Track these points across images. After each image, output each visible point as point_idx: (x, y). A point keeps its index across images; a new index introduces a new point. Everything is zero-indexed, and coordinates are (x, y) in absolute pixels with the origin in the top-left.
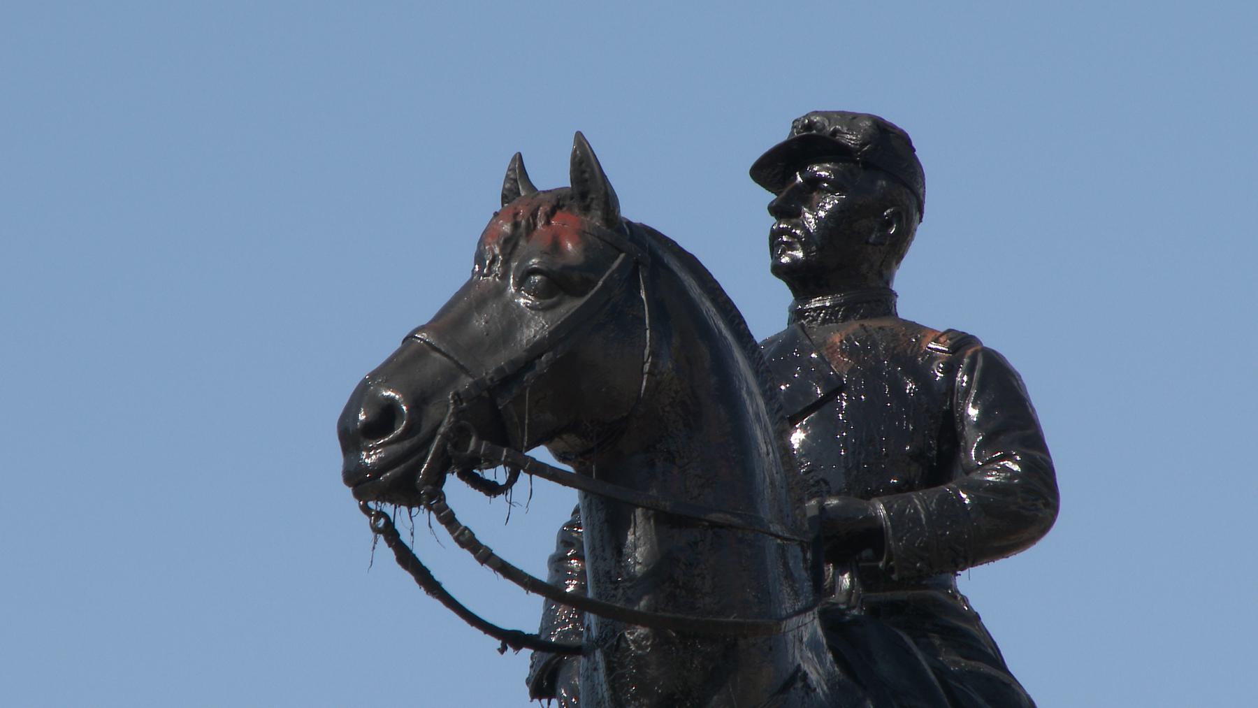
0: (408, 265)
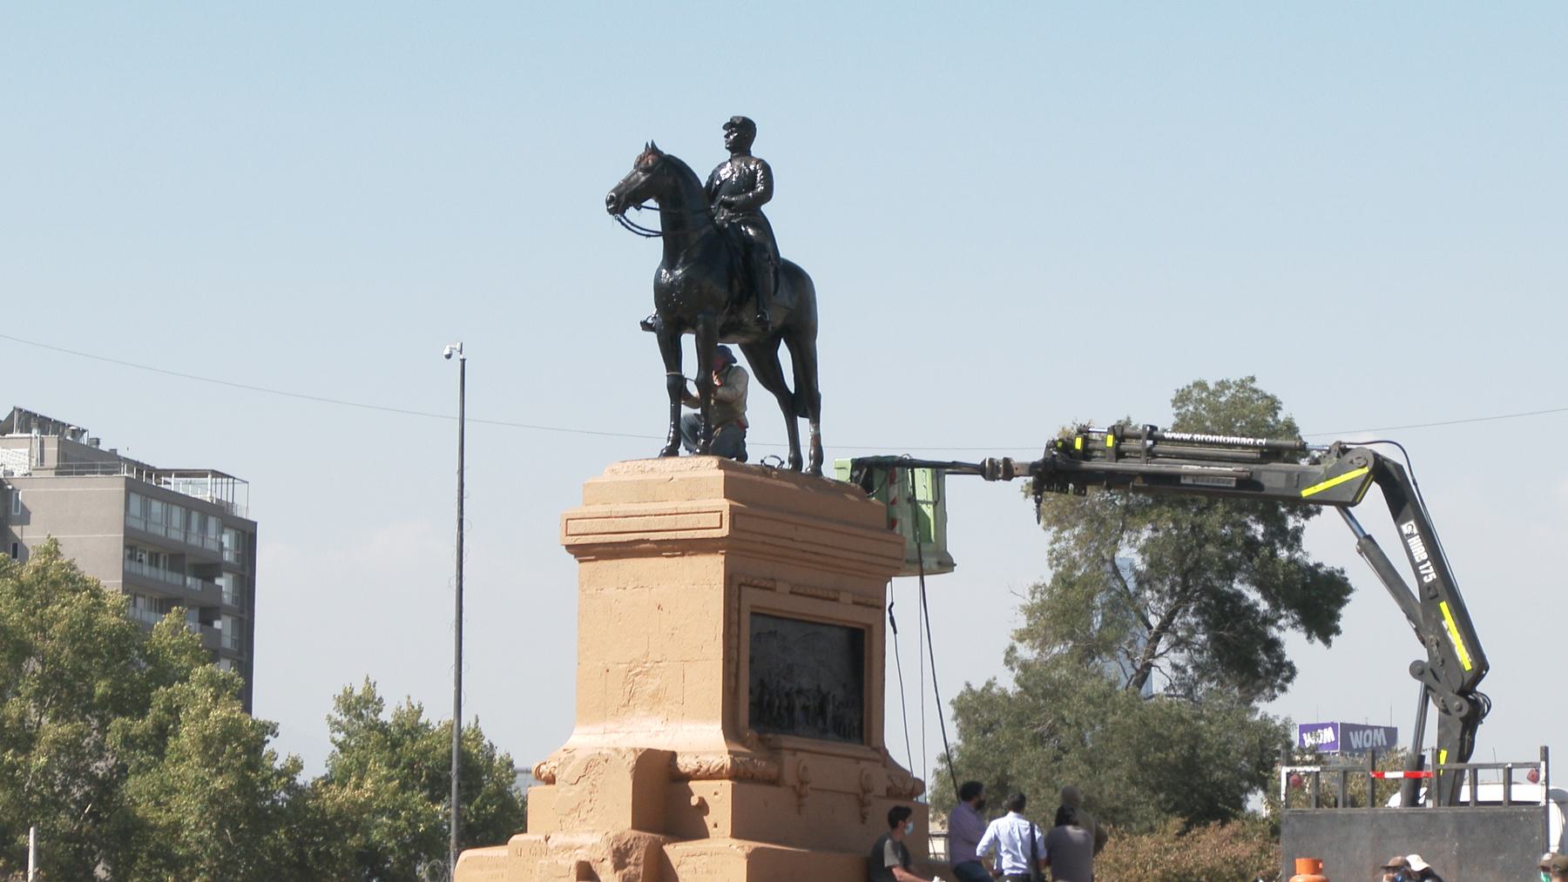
0: (622, 167)
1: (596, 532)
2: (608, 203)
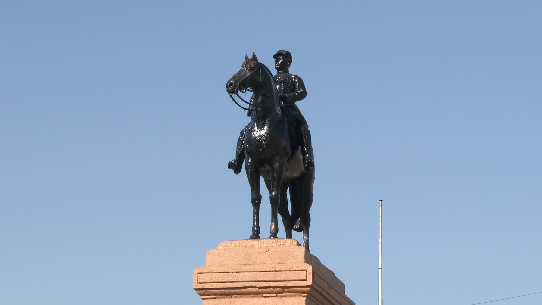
0: (235, 67)
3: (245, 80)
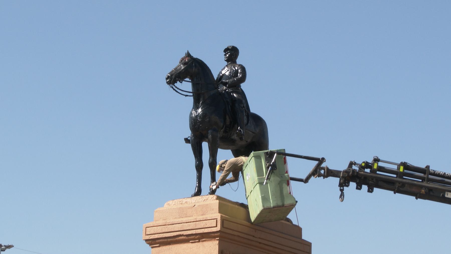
0: (174, 63)
1: (158, 232)
2: (167, 79)
3: (180, 72)
